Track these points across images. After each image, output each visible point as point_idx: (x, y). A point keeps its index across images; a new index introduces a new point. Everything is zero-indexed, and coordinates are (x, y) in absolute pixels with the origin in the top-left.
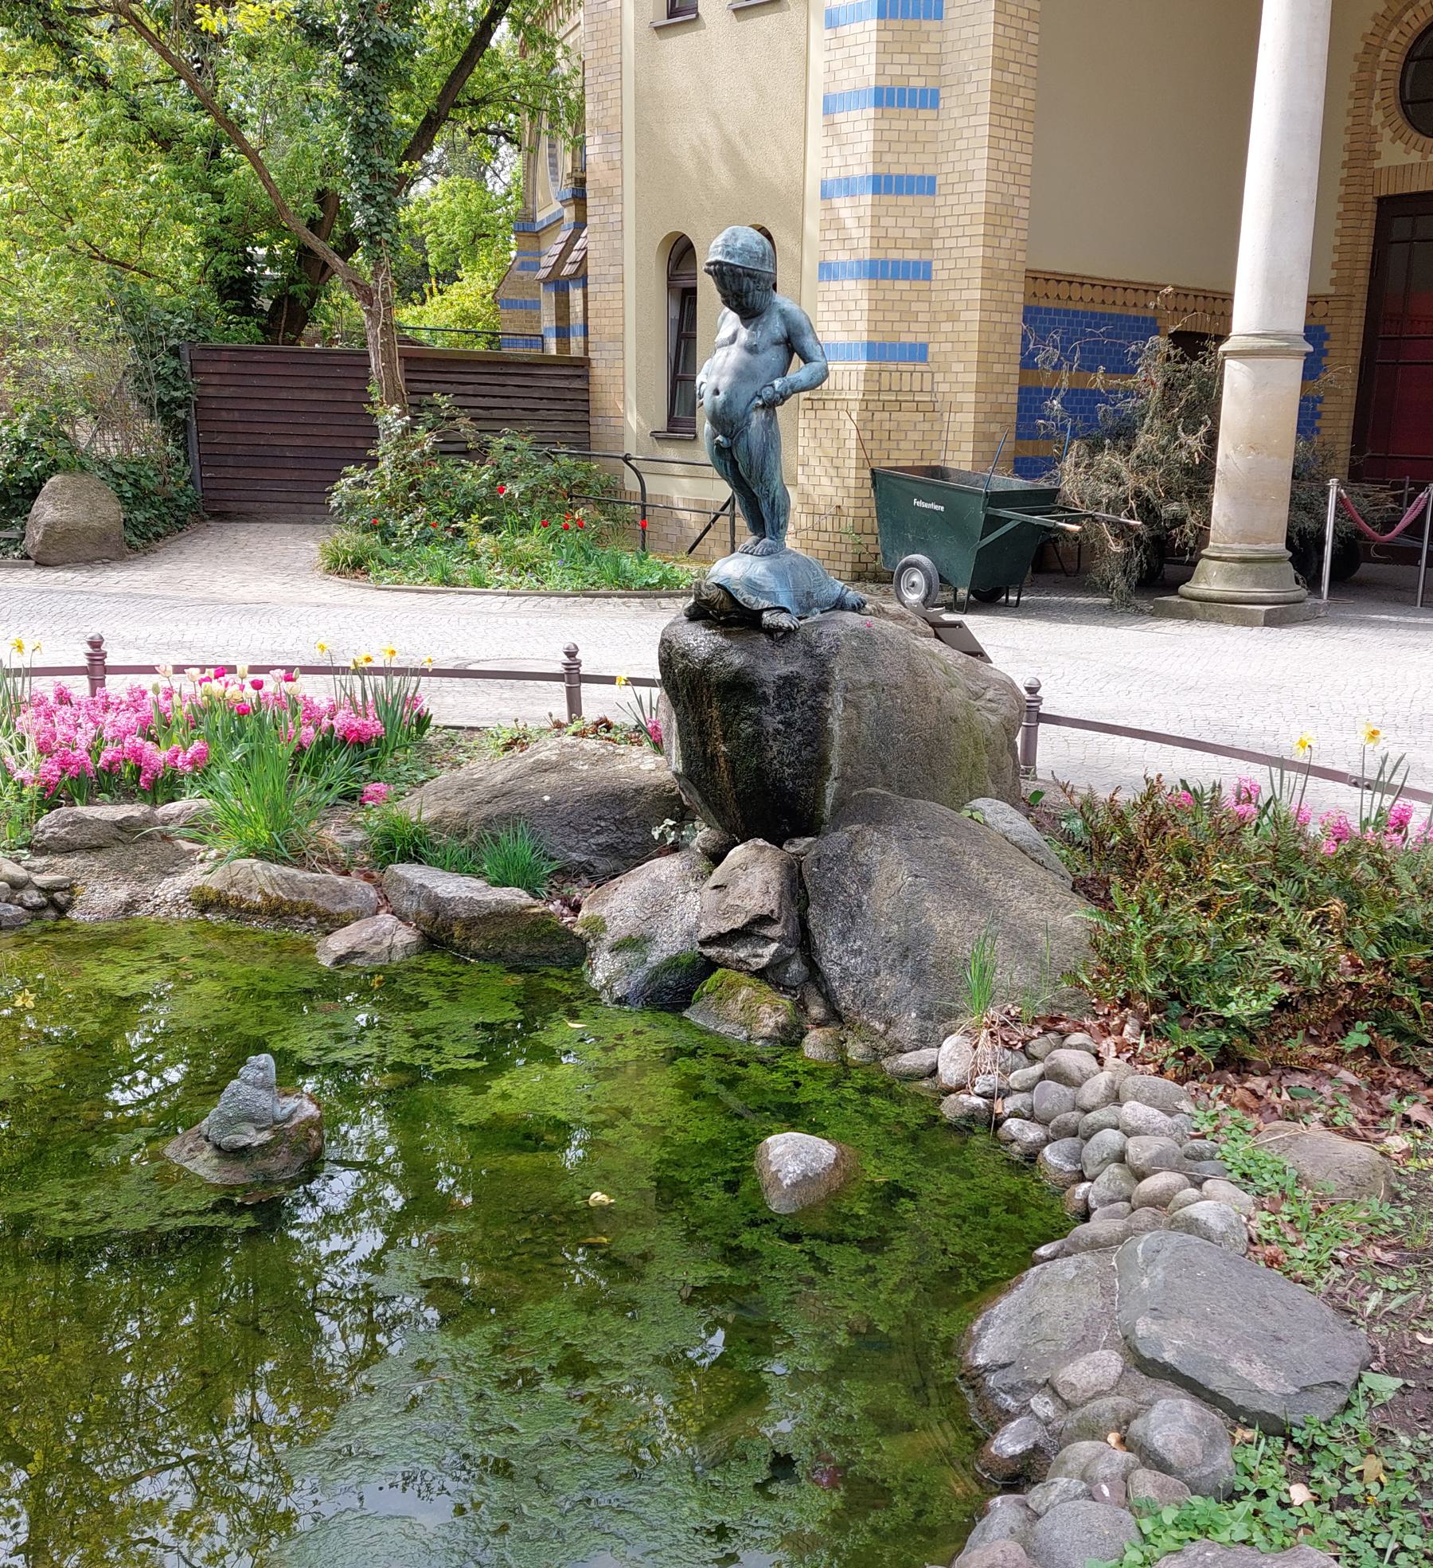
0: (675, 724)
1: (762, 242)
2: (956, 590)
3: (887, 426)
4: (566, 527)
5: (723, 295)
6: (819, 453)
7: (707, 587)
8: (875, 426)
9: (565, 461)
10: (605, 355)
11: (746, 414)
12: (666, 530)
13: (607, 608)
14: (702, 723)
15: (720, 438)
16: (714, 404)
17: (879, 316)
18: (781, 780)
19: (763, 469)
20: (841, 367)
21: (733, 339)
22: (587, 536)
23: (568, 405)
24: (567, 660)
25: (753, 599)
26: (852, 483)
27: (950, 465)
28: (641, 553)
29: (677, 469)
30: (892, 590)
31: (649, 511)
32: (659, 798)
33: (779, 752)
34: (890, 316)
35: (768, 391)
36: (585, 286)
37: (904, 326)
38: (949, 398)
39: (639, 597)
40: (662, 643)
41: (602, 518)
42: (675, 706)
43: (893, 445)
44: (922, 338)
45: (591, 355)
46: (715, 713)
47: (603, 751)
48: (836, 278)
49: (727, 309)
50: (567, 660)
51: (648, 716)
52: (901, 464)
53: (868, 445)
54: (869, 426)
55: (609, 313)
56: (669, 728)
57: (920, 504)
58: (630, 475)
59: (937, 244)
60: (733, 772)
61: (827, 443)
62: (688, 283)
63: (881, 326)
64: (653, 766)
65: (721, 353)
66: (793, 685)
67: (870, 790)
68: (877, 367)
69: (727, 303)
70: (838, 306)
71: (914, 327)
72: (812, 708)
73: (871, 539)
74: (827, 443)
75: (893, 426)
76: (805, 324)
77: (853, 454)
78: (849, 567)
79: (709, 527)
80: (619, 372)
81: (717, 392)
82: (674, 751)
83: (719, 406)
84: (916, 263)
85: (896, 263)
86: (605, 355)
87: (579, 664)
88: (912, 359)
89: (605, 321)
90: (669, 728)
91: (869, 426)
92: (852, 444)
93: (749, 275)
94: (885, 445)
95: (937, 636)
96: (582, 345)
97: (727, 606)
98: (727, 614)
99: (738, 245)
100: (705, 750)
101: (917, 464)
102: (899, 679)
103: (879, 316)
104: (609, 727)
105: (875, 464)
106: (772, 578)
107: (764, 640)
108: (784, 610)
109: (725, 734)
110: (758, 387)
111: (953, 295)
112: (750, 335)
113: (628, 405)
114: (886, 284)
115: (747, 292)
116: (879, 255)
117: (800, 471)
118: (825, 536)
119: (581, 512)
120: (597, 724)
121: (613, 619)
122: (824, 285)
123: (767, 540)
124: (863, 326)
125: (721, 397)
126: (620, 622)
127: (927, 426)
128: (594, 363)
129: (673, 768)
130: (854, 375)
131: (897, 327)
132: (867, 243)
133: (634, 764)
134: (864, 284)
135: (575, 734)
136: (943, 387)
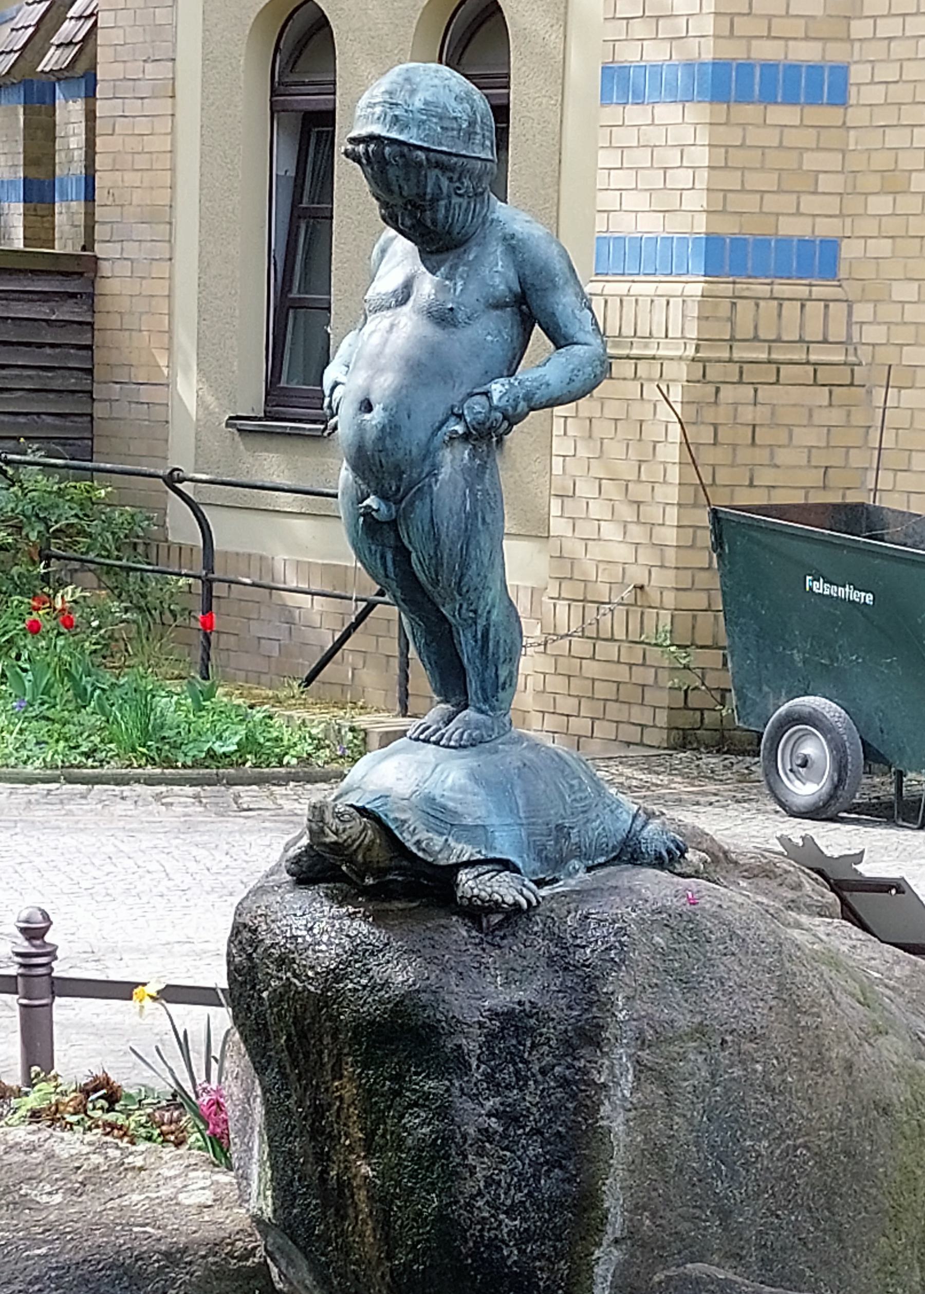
0: (259, 1109)
1: (467, 98)
2: (900, 775)
3: (747, 414)
4: (34, 628)
5: (384, 205)
6: (597, 470)
7: (338, 816)
8: (722, 414)
9: (35, 479)
10: (131, 250)
11: (428, 453)
12: (256, 629)
13: (120, 808)
14: (319, 1111)
15: (372, 501)
16: (361, 429)
17: (732, 180)
18: (495, 1245)
19: (464, 566)
20: (649, 289)
21: (404, 294)
22: (79, 644)
23: (46, 357)
24: (24, 946)
25: (438, 842)
26: (670, 536)
27: (891, 502)
28: (201, 685)
29: (284, 501)
30: (758, 771)
31: (219, 589)
32: (220, 1273)
33: (490, 1181)
34: (756, 181)
35: (478, 405)
36: (90, 95)
37: (787, 202)
38: (887, 355)
39: (193, 782)
40: (237, 930)
41: (115, 606)
42: (260, 1070)
43: (762, 456)
44: (826, 228)
45: (99, 250)
46: (349, 1091)
47: (96, 1159)
48: (639, 100)
49: (392, 232)
50: (24, 946)
51: (201, 1078)
52: (781, 498)
53: (707, 457)
54: (709, 415)
55: (142, 162)
56: (246, 1115)
57: (819, 587)
58: (178, 511)
59: (860, 28)
60: (384, 1222)
61: (615, 449)
62: (315, 102)
63: (737, 203)
64: (207, 1197)
65: (378, 323)
66: (522, 1032)
67: (693, 1268)
68: (727, 289)
69: (391, 219)
70: (642, 157)
71: (809, 204)
72: (564, 1083)
73: (713, 658)
74: (615, 449)
75: (761, 414)
76: (558, 265)
77: (674, 474)
78: (662, 718)
79: (354, 626)
80: (161, 288)
81: (367, 406)
82: (255, 1169)
83: (371, 435)
84: (815, 70)
85: (769, 68)
86: (131, 250)
87: (52, 954)
88: (805, 271)
89: (131, 178)
90: (246, 1115)
91: (709, 415)
92: (671, 452)
93: (438, 165)
94: (745, 455)
95: (850, 914)
96: (80, 219)
97: (380, 855)
98: (380, 872)
99: (418, 104)
100: (325, 1171)
101: (817, 498)
102: (760, 1018)
103: (732, 180)
104: (112, 1097)
105: (720, 500)
106: (482, 795)
107: (461, 930)
108: (506, 865)
109: (370, 1136)
110: (455, 396)
111: (894, 138)
112: (440, 288)
113: (179, 358)
114: (751, 112)
115: (435, 199)
116: (734, 51)
117: (555, 509)
118: (608, 650)
119: (69, 593)
120: (85, 1092)
121: (131, 833)
122: (611, 114)
123: (469, 714)
124: (696, 200)
125: (376, 417)
126: (146, 841)
127: (835, 416)
128: (105, 268)
129: (253, 1205)
130: (676, 303)
131: (772, 203)
132: (708, 26)
133: (164, 1192)
134: (699, 112)
135: (35, 1115)
136: (874, 334)
